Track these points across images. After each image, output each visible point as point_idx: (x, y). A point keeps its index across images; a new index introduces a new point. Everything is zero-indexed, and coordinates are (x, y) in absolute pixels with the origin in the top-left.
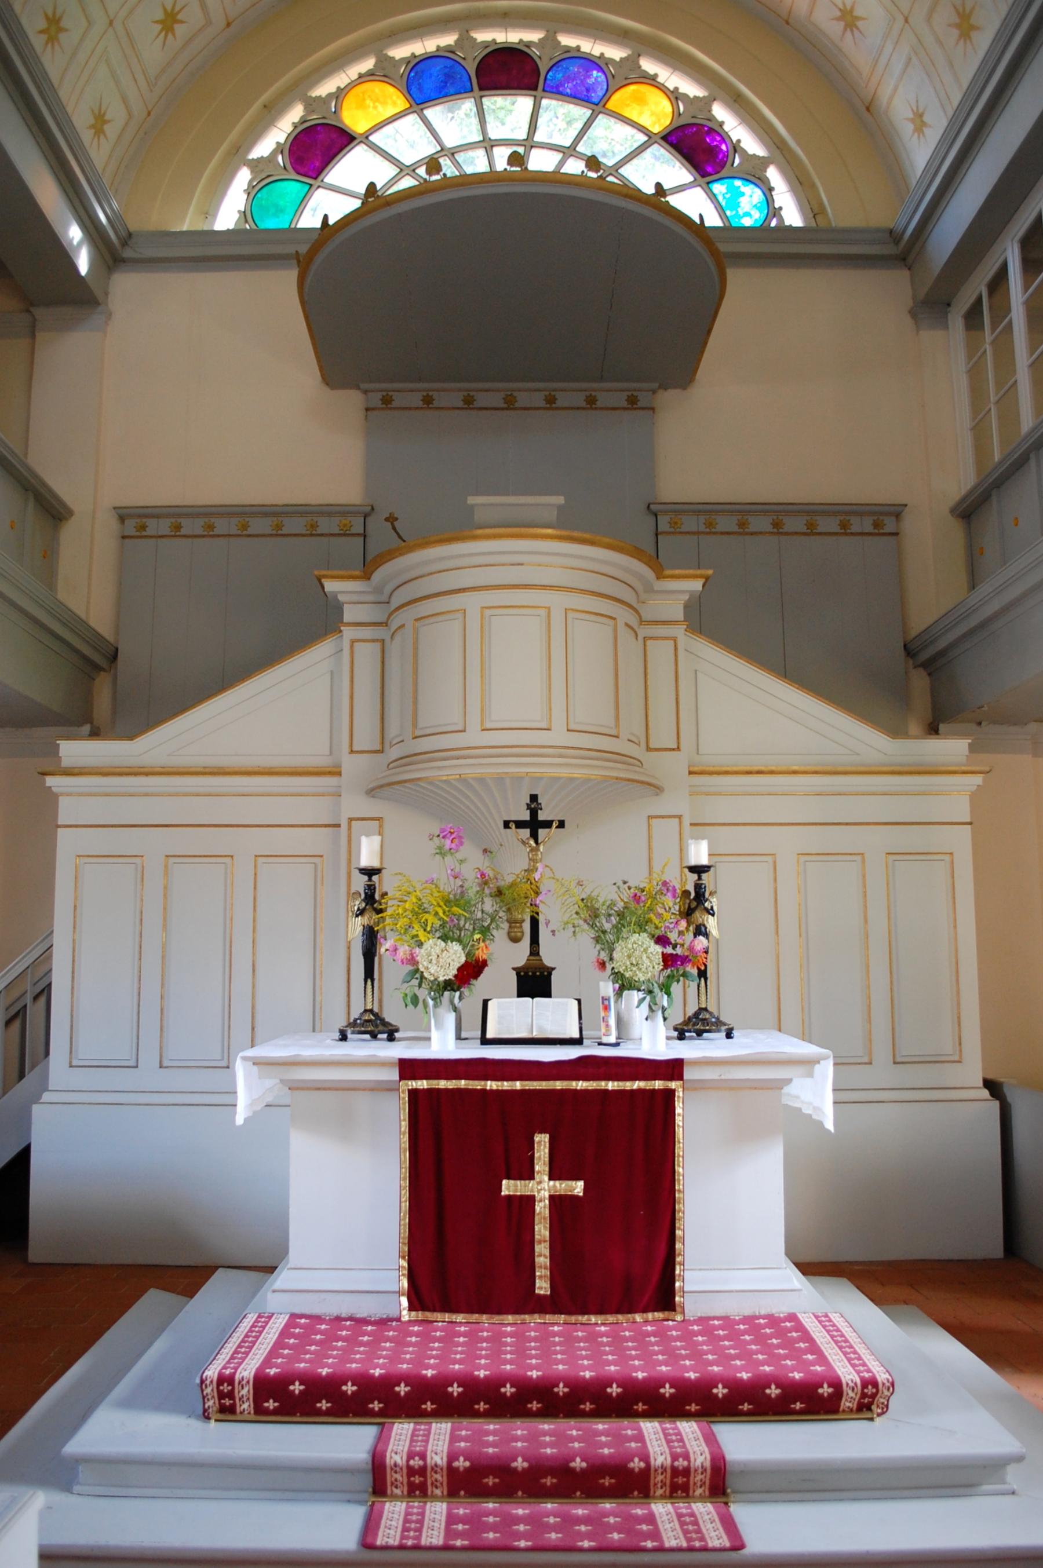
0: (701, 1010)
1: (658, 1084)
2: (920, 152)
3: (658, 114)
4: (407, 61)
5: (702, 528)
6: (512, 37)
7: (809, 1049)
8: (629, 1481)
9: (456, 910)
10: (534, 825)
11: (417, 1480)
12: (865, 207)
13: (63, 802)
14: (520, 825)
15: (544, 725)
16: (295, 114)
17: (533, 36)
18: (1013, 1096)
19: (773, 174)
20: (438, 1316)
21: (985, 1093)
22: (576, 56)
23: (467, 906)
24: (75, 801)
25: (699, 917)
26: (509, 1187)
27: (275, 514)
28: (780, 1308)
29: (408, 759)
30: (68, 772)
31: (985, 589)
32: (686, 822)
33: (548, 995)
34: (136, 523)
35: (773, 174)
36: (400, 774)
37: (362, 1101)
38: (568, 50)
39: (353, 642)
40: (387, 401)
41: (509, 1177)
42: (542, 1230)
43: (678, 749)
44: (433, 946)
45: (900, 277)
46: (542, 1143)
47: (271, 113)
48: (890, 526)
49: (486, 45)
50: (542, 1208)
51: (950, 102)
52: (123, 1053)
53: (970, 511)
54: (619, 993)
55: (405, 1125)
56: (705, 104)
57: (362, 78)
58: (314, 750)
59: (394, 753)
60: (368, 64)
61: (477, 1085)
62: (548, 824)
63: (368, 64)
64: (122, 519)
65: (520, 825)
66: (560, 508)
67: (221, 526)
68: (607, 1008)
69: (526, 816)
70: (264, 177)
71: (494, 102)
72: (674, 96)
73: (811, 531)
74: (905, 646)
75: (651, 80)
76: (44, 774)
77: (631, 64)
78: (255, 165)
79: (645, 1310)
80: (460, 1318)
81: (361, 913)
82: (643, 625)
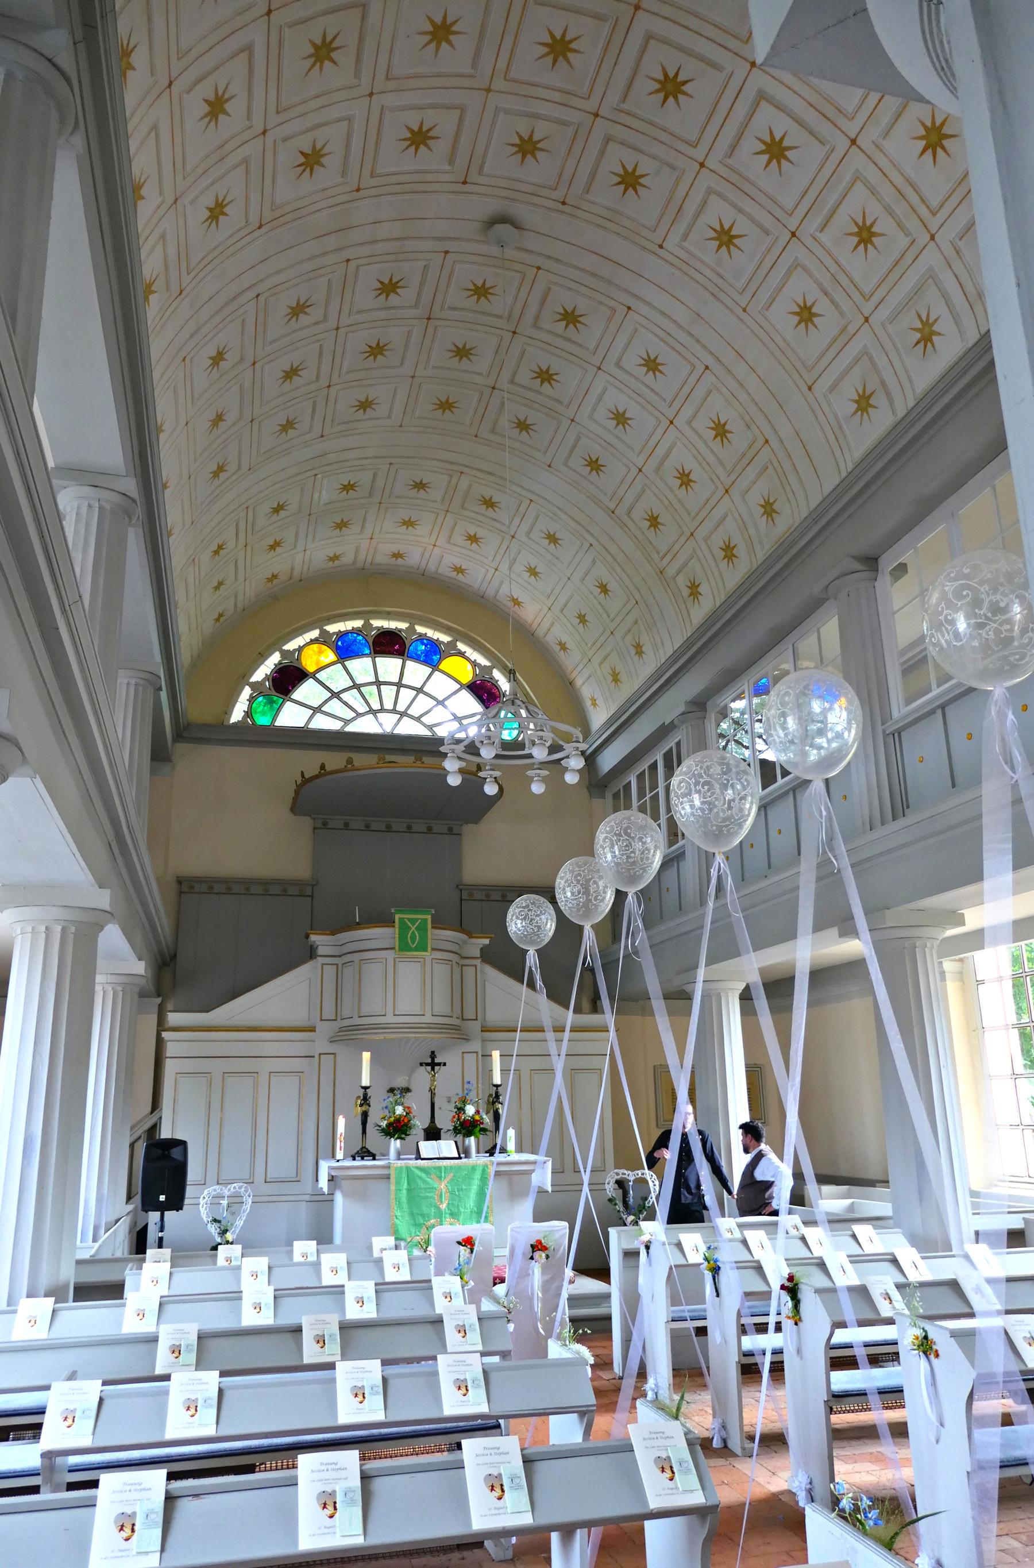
3: (467, 675)
4: (337, 634)
10: (433, 1065)
16: (275, 658)
17: (403, 625)
22: (422, 638)
38: (420, 635)
40: (325, 824)
47: (263, 657)
49: (378, 628)
56: (489, 670)
57: (313, 641)
58: (299, 1016)
60: (315, 634)
62: (439, 1064)
63: (315, 634)
65: (427, 1064)
69: (429, 1061)
71: (382, 662)
72: (474, 664)
75: (462, 654)
77: (452, 645)
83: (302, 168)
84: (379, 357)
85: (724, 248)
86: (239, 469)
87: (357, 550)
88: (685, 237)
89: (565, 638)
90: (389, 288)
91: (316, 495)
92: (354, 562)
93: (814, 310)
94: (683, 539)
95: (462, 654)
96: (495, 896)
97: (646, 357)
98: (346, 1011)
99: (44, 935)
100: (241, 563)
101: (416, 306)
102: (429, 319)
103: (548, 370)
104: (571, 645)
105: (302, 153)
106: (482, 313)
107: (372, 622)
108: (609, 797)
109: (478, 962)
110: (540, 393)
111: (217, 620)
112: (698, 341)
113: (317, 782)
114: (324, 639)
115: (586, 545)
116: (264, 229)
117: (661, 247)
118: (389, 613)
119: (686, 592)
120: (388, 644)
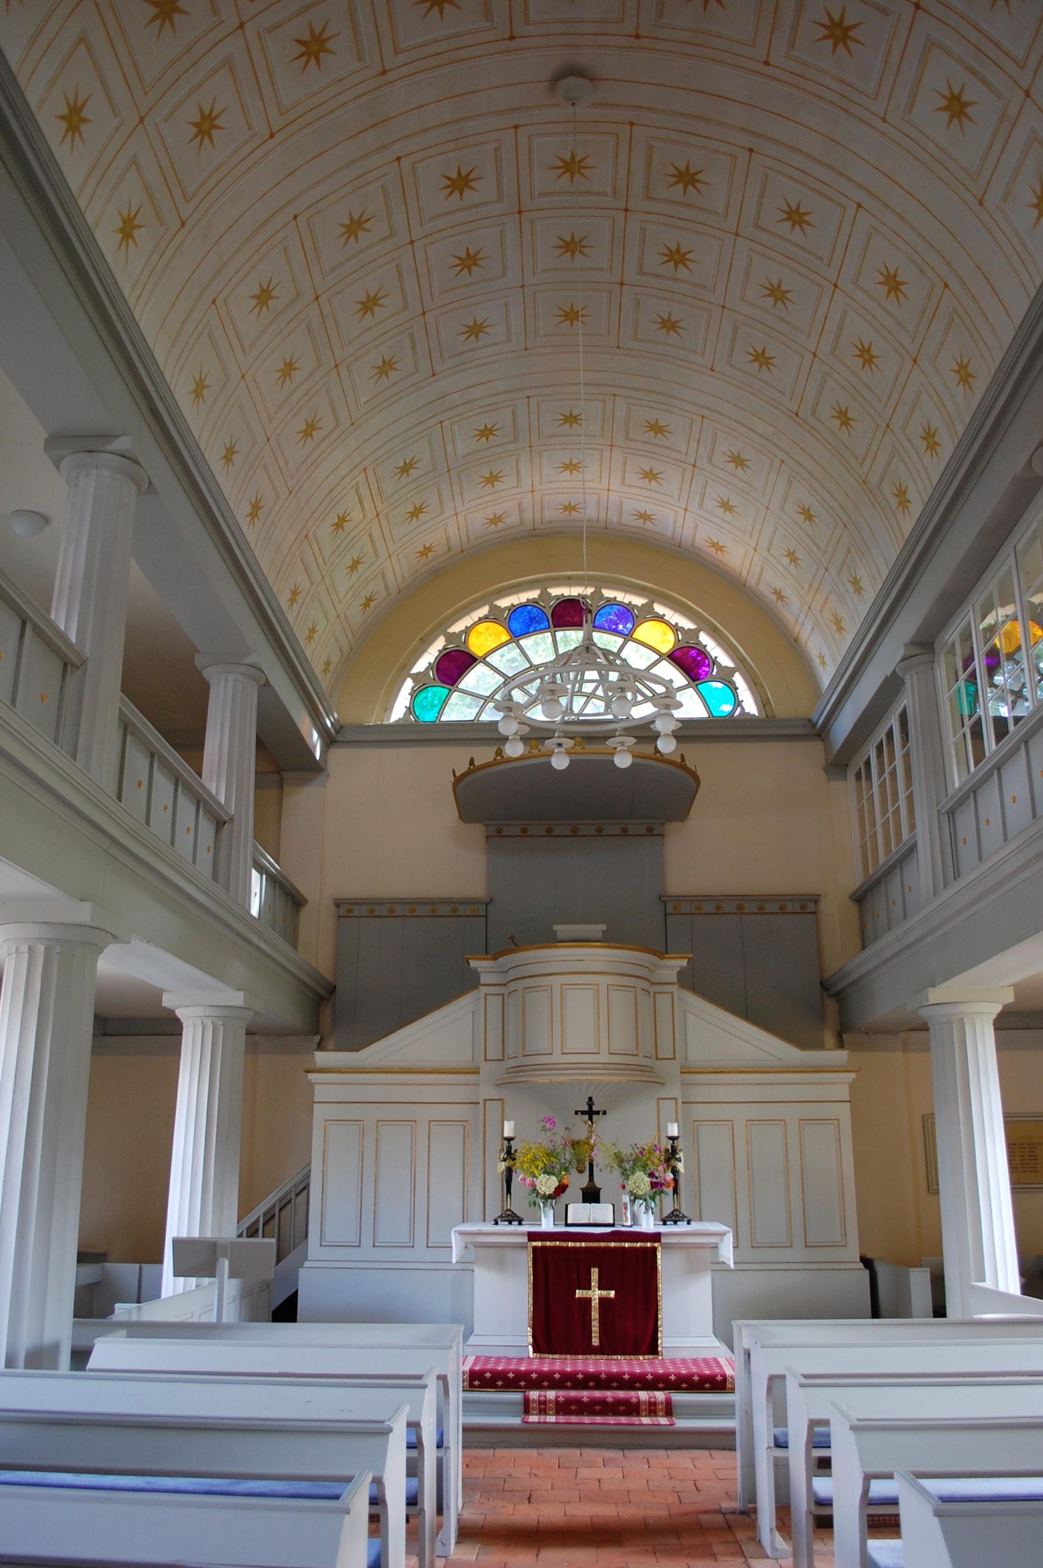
0: (675, 1210)
1: (649, 1244)
2: (826, 676)
3: (666, 642)
4: (509, 608)
5: (694, 911)
6: (574, 591)
7: (727, 1228)
8: (632, 1409)
9: (553, 1159)
10: (590, 1113)
11: (542, 1407)
12: (791, 705)
13: (317, 1088)
14: (583, 1113)
15: (595, 1051)
16: (440, 644)
18: (881, 1269)
19: (738, 678)
20: (546, 1356)
21: (861, 1265)
22: (611, 602)
23: (556, 1156)
24: (325, 1089)
25: (673, 1162)
26: (579, 1294)
27: (433, 903)
28: (709, 1355)
29: (519, 1069)
30: (322, 1071)
31: (868, 952)
32: (680, 1102)
33: (598, 1202)
34: (346, 909)
35: (738, 678)
36: (518, 1074)
37: (510, 1253)
38: (609, 600)
39: (486, 995)
40: (499, 831)
41: (579, 1289)
42: (595, 1315)
43: (674, 1058)
44: (543, 1178)
45: (814, 750)
46: (595, 1273)
48: (811, 907)
49: (557, 597)
50: (595, 1303)
51: (879, 574)
52: (352, 1238)
53: (861, 898)
54: (633, 1202)
55: (530, 1264)
56: (695, 633)
57: (481, 620)
58: (460, 1053)
59: (512, 1063)
60: (484, 611)
61: (564, 1244)
62: (598, 1113)
63: (484, 611)
64: (337, 905)
65: (583, 1113)
66: (603, 931)
67: (399, 910)
68: (626, 1208)
69: (586, 1108)
70: (421, 684)
72: (676, 628)
73: (761, 912)
74: (821, 984)
75: (660, 618)
76: (308, 1072)
77: (648, 608)
78: (416, 677)
79: (644, 1354)
80: (557, 1356)
81: (505, 1160)
82: (652, 985)
83: (305, 58)
84: (474, 269)
85: (841, 46)
86: (337, 425)
87: (521, 510)
88: (791, 45)
89: (779, 584)
90: (460, 183)
91: (450, 447)
92: (522, 523)
93: (965, 98)
94: (879, 436)
95: (660, 618)
96: (729, 907)
97: (786, 209)
98: (510, 1051)
99: (26, 956)
100: (377, 536)
101: (500, 199)
102: (520, 212)
103: (678, 250)
104: (788, 592)
105: (299, 41)
106: (581, 193)
107: (550, 590)
108: (851, 777)
109: (675, 988)
110: (676, 280)
111: (366, 605)
112: (841, 174)
113: (468, 779)
114: (494, 616)
115: (777, 463)
116: (278, 138)
117: (767, 63)
118: (569, 578)
119: (894, 502)
120: (568, 614)
